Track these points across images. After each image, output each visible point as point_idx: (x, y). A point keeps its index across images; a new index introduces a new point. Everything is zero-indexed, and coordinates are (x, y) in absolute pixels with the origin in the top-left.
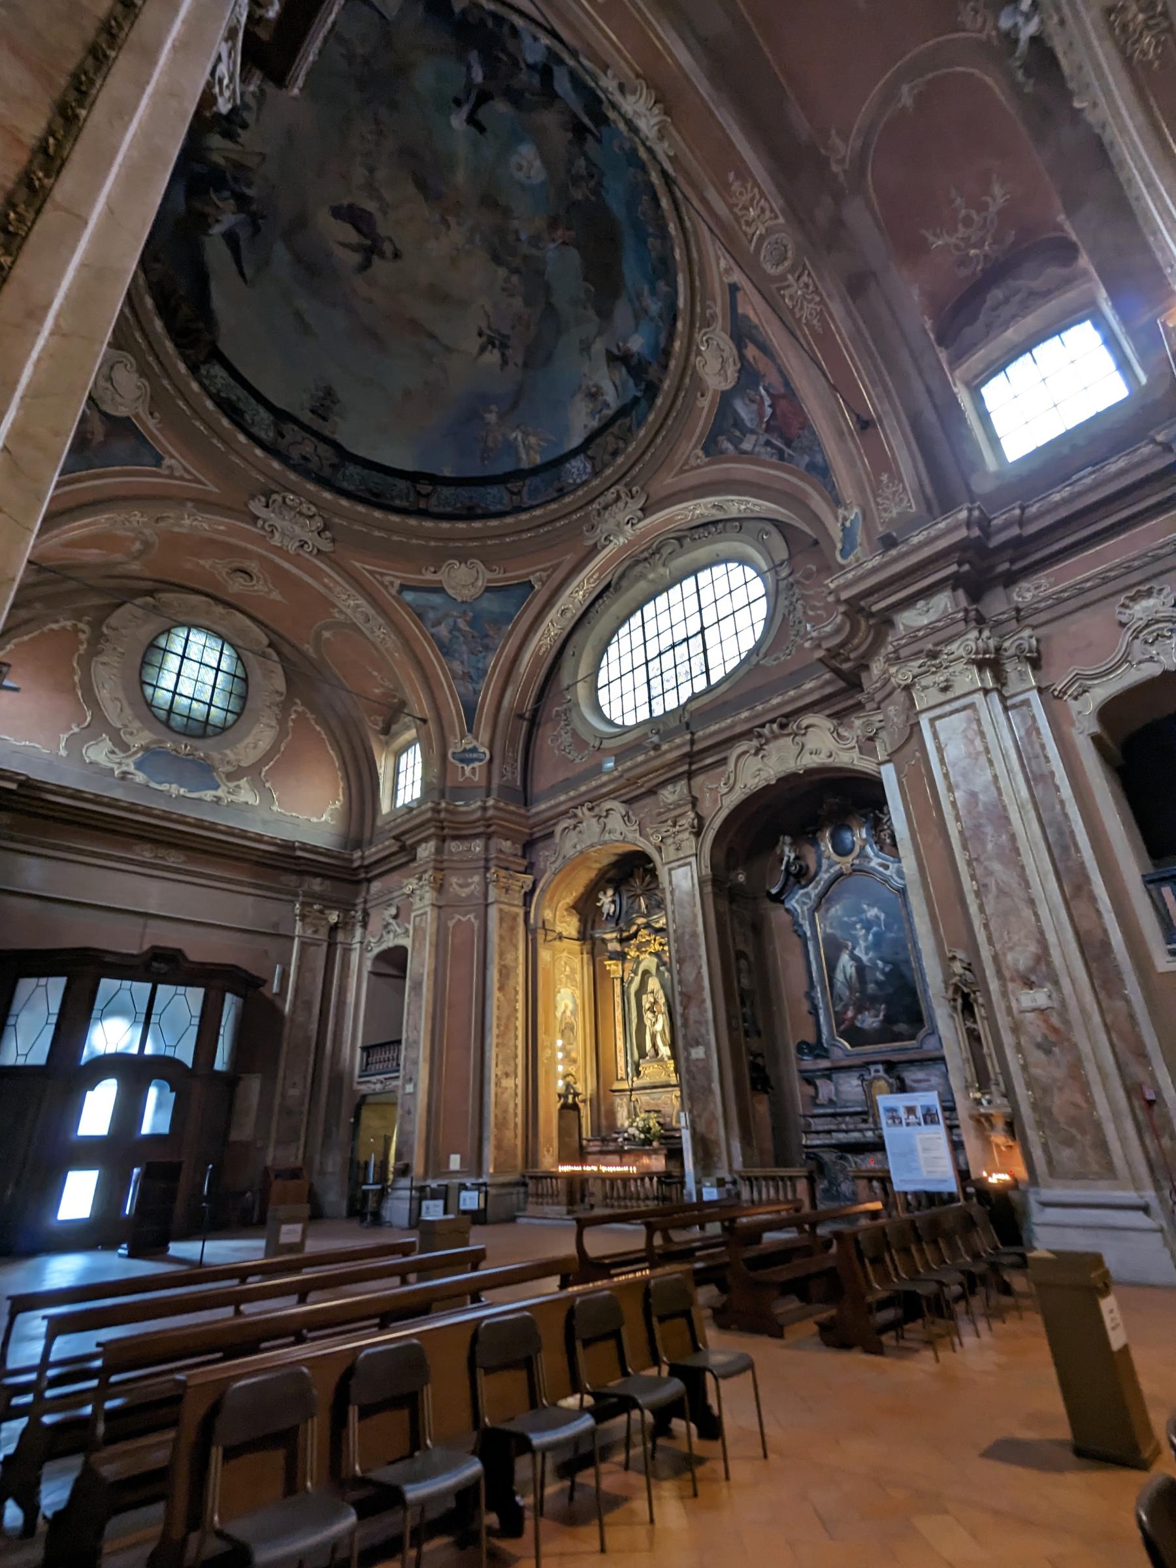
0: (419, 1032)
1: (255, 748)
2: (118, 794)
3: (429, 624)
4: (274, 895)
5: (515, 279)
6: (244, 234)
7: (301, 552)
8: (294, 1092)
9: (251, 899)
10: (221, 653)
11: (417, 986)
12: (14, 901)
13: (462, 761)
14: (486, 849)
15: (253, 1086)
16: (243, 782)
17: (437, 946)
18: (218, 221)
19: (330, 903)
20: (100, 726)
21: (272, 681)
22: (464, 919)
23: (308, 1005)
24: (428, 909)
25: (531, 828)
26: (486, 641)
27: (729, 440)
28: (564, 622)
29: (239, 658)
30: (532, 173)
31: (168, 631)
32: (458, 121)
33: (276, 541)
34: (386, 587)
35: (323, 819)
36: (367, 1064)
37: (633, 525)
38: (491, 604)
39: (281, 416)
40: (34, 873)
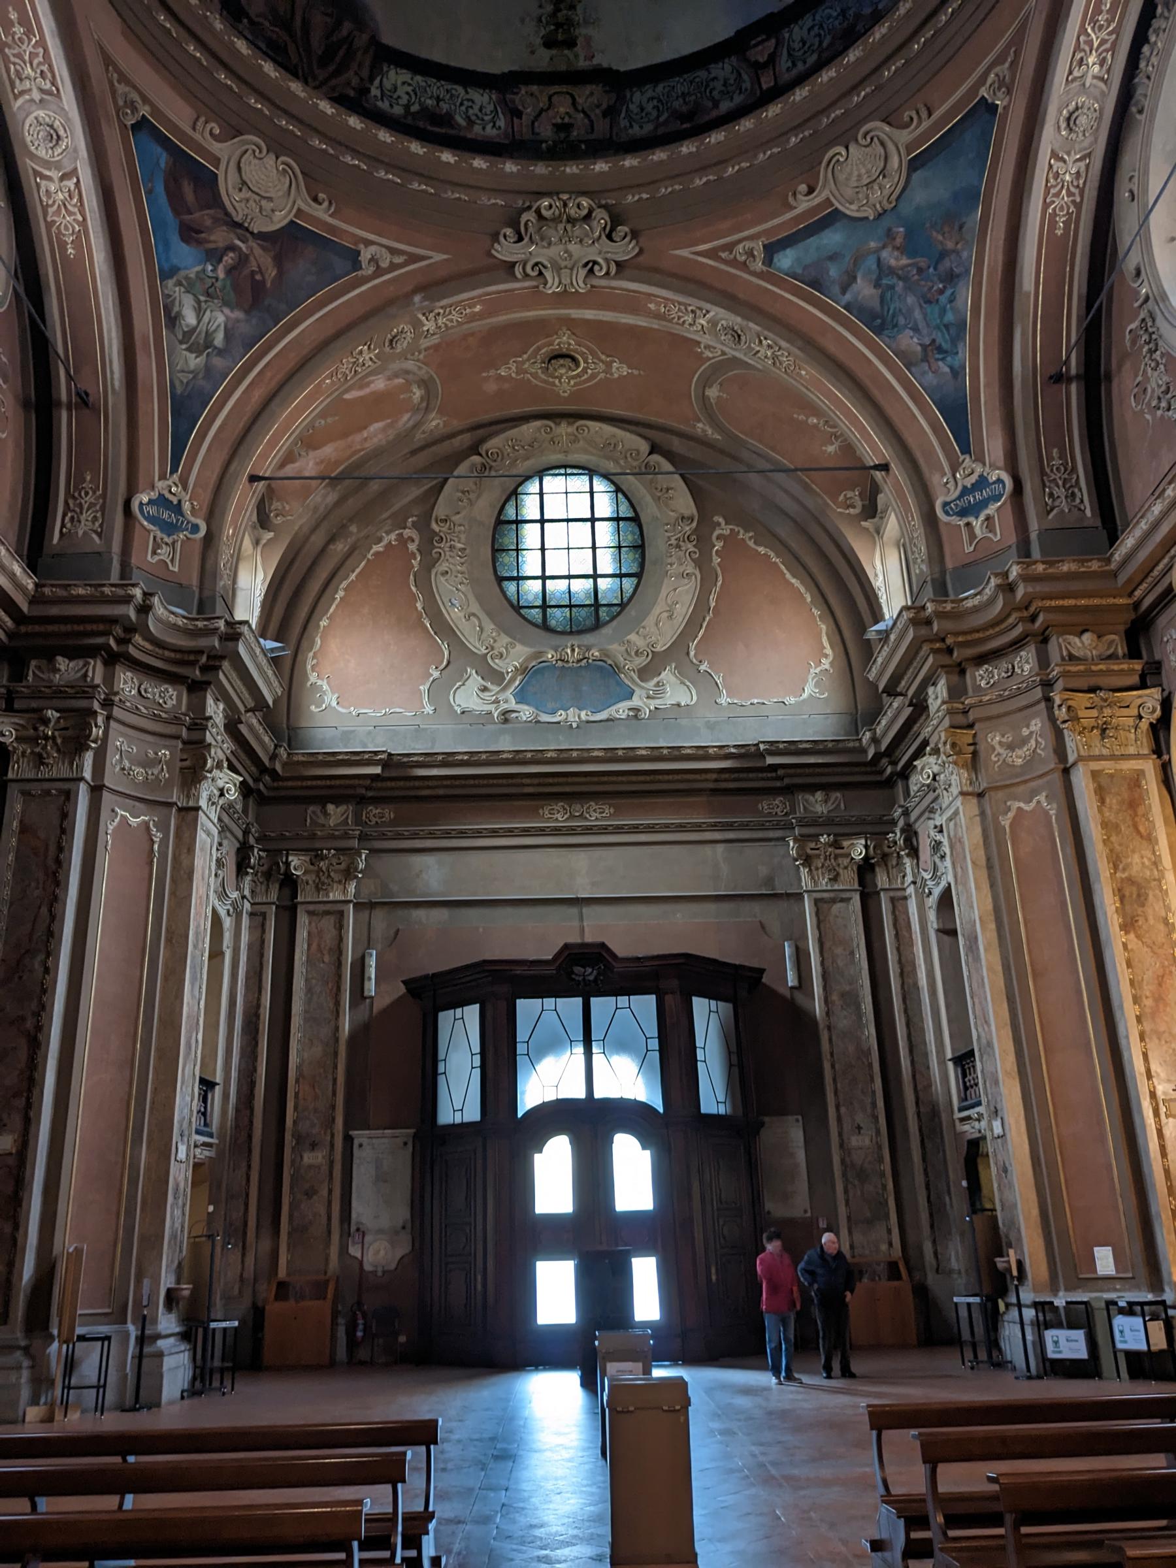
0: (989, 1025)
1: (670, 617)
2: (505, 744)
3: (836, 289)
4: (760, 835)
7: (596, 282)
8: (860, 1142)
9: (720, 848)
10: (592, 493)
11: (973, 940)
12: (420, 914)
13: (963, 513)
14: (1043, 661)
15: (790, 1136)
16: (667, 675)
17: (990, 867)
19: (842, 829)
20: (462, 659)
22: (1027, 808)
23: (851, 999)
24: (959, 802)
25: (1130, 595)
26: (947, 264)
28: (1083, 142)
29: (618, 490)
31: (514, 494)
33: (553, 286)
34: (744, 266)
35: (805, 695)
36: (966, 1088)
38: (931, 191)
39: (502, 84)
40: (432, 873)
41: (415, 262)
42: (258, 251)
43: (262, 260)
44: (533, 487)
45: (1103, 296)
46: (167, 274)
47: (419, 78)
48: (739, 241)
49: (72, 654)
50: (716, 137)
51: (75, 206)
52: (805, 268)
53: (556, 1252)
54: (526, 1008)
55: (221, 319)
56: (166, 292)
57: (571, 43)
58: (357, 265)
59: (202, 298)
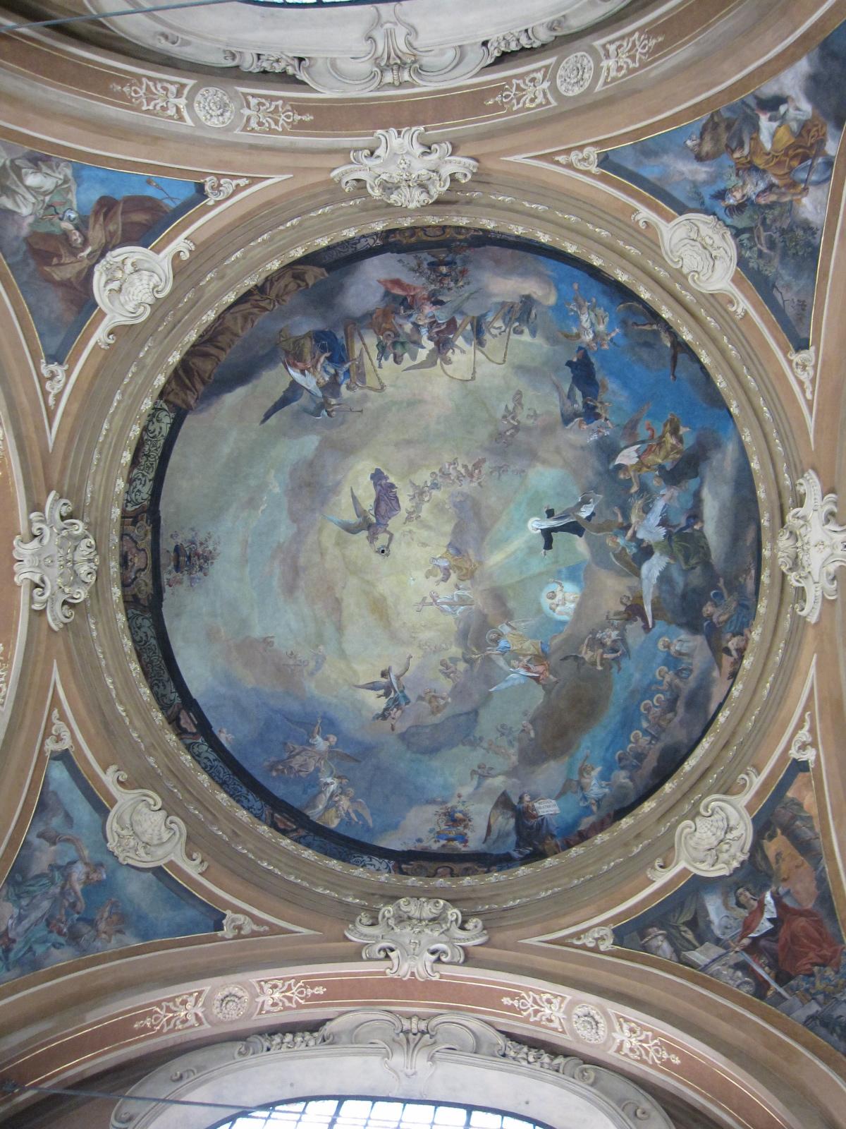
3: (41, 827)
5: (462, 666)
6: (303, 401)
18: (303, 372)
26: (84, 928)
27: (669, 938)
30: (559, 609)
32: (536, 525)
34: (47, 734)
37: (439, 960)
41: (48, 415)
42: (78, 267)
43: (67, 271)
45: (84, 1094)
47: (162, 442)
48: (69, 726)
50: (145, 692)
51: (270, 104)
52: (55, 793)
55: (25, 211)
56: (62, 164)
58: (52, 359)
59: (47, 198)
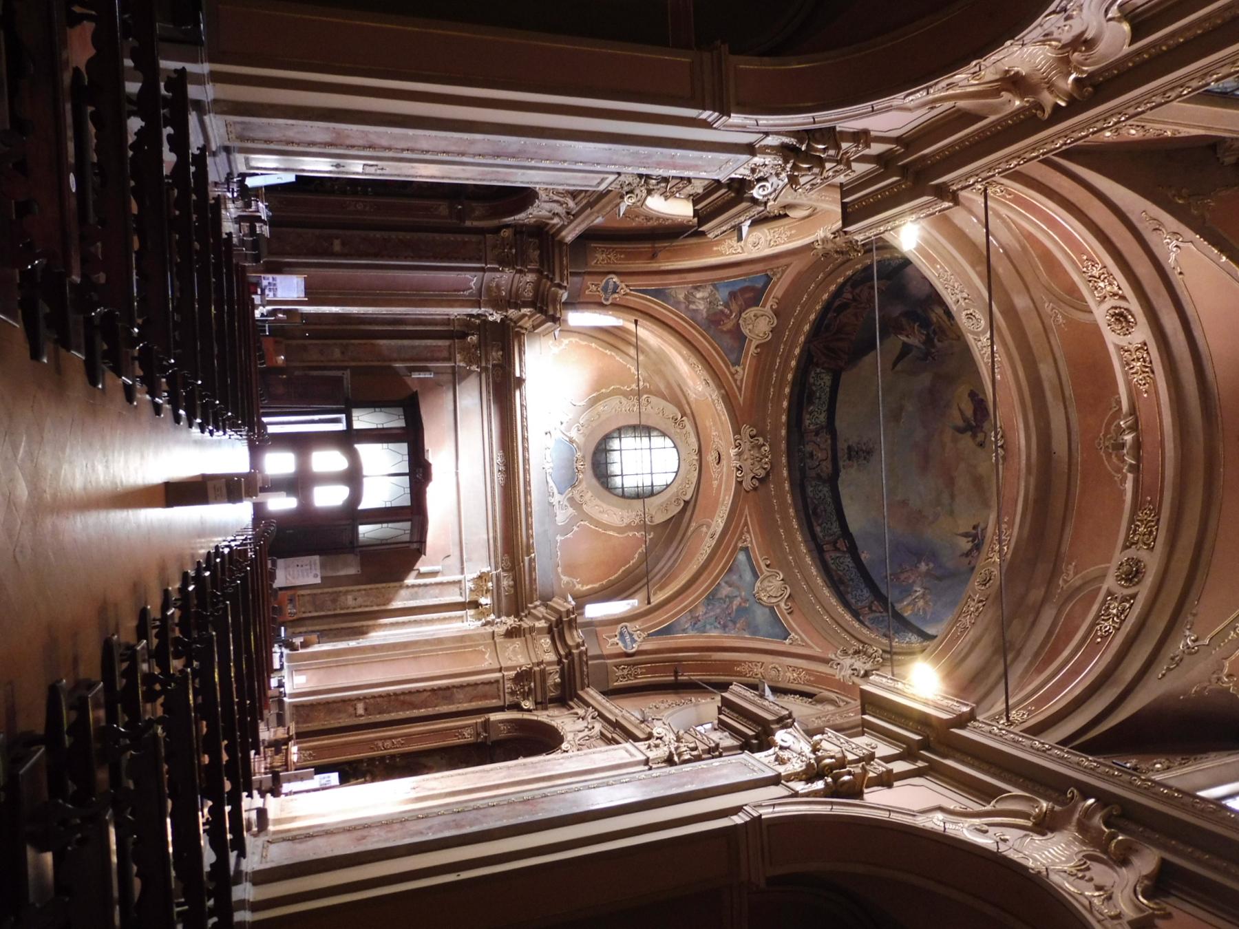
8: (350, 600)
13: (621, 634)
14: (550, 663)
16: (571, 510)
21: (658, 512)
26: (730, 624)
29: (668, 486)
38: (761, 615)
43: (729, 325)
44: (669, 443)
46: (714, 286)
49: (541, 256)
53: (300, 502)
54: (403, 448)
55: (701, 307)
57: (850, 458)
58: (734, 365)
